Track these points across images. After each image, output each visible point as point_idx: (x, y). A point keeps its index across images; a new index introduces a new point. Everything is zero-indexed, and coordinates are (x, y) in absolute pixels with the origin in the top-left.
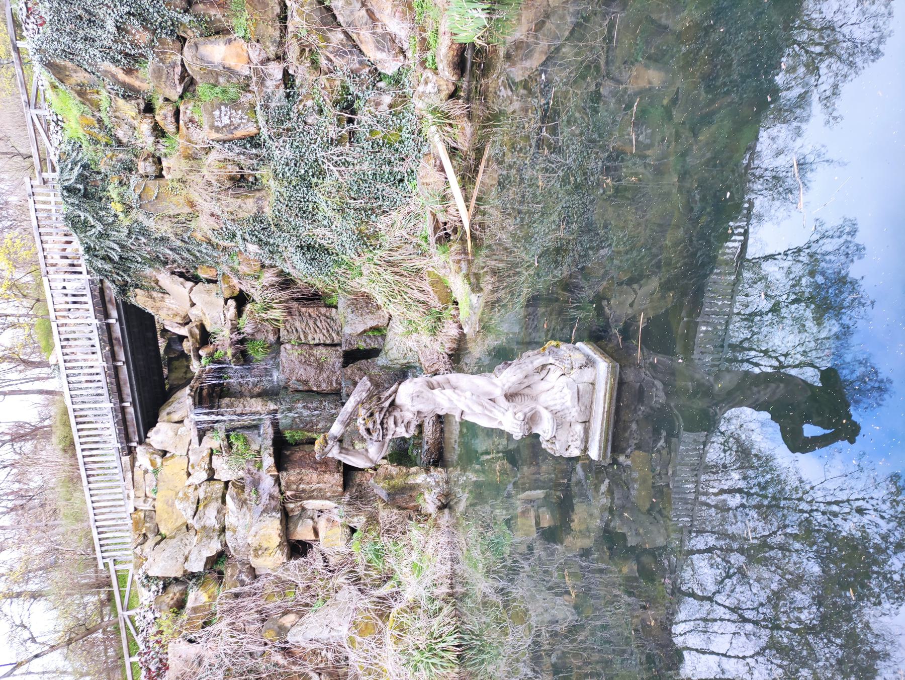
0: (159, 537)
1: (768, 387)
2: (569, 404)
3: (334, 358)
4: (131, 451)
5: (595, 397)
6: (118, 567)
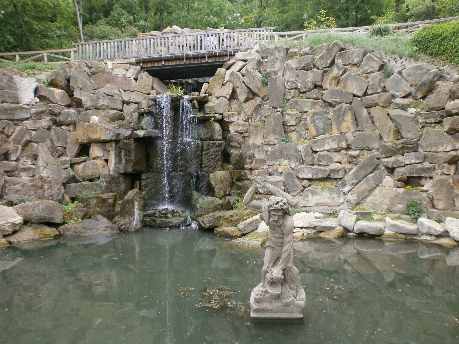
0: (90, 74)
4: (138, 63)
5: (411, 233)
6: (72, 53)
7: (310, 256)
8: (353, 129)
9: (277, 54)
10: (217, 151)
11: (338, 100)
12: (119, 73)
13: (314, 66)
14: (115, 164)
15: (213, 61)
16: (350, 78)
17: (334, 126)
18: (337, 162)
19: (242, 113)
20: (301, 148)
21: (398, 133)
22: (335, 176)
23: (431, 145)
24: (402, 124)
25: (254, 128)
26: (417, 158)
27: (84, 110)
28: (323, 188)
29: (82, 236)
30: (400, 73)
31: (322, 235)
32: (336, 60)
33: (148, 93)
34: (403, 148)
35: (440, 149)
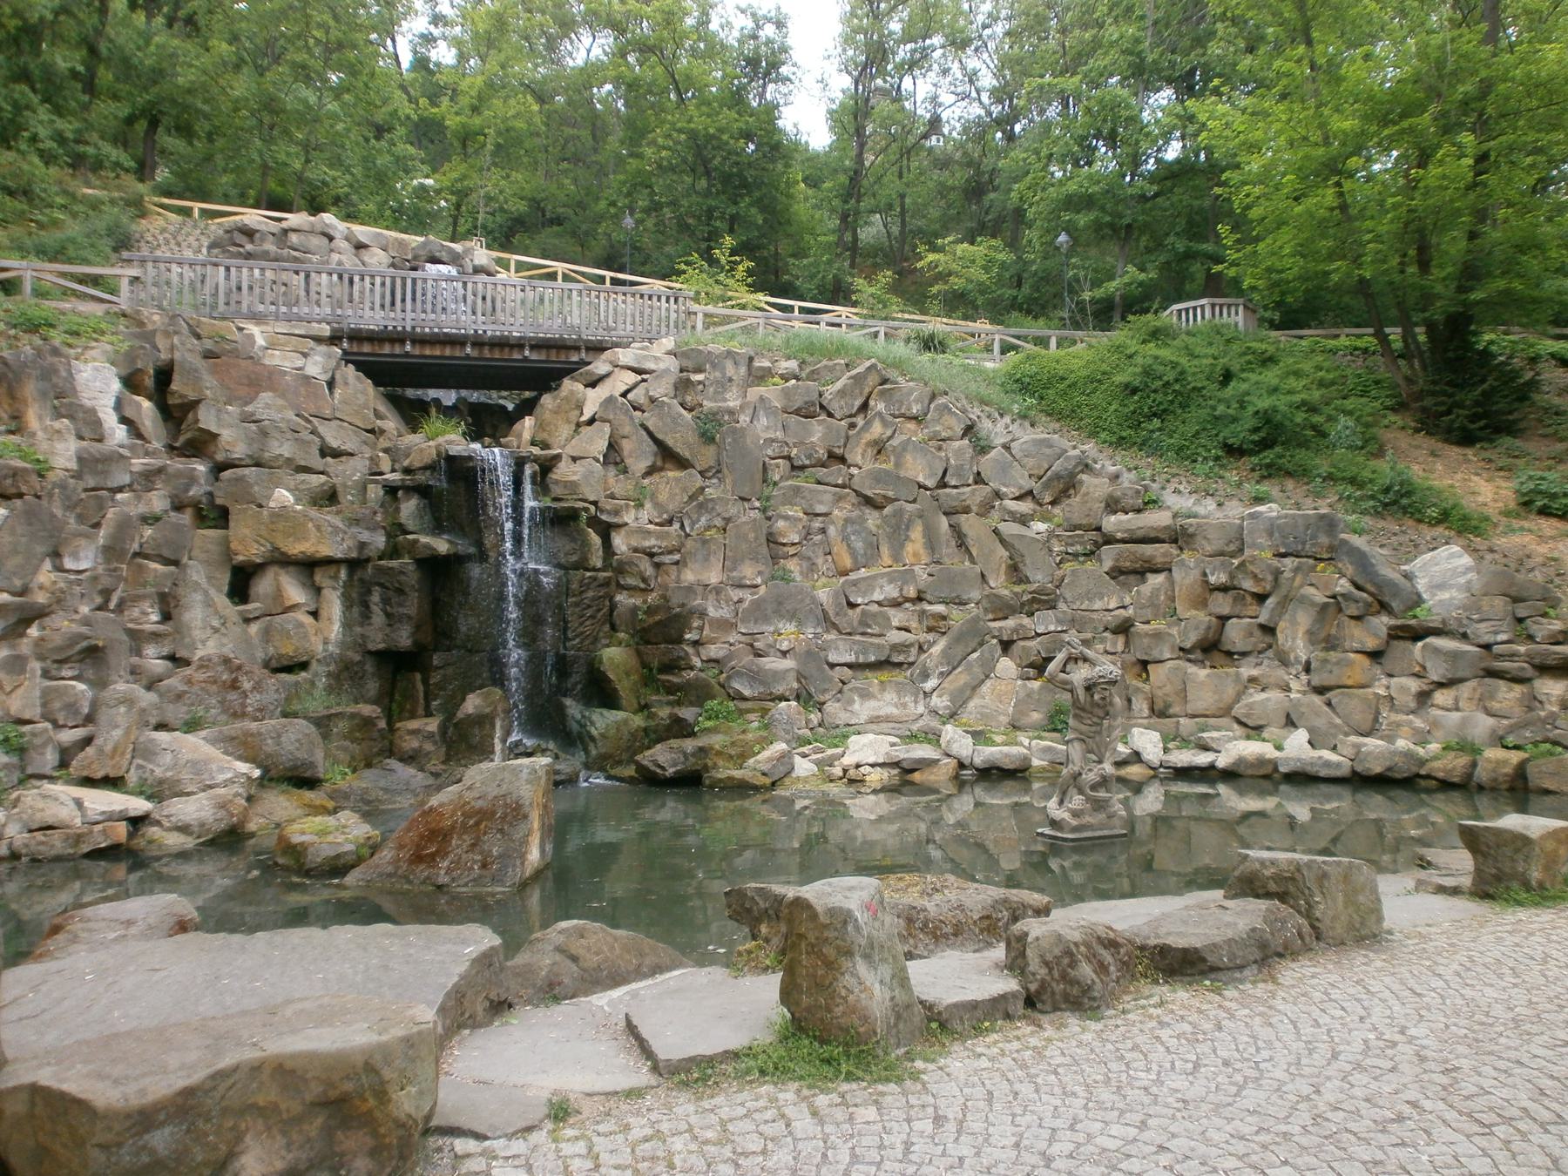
4: (334, 339)
6: (124, 283)
7: (859, 833)
8: (925, 559)
9: (730, 370)
11: (890, 494)
12: (283, 360)
13: (822, 407)
14: (347, 625)
15: (543, 357)
16: (910, 447)
17: (885, 551)
18: (899, 629)
19: (648, 505)
20: (823, 595)
21: (1015, 571)
22: (901, 658)
23: (1081, 597)
24: (1025, 552)
25: (699, 545)
26: (1059, 622)
28: (882, 682)
29: (384, 812)
30: (1007, 447)
31: (917, 776)
32: (872, 403)
34: (1034, 600)
35: (1098, 605)
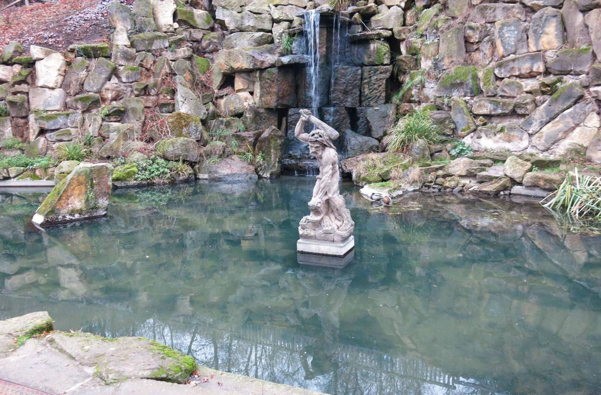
1: (331, 335)
2: (324, 229)
3: (349, 102)
10: (381, 79)
27: (229, 33)
33: (304, 6)
